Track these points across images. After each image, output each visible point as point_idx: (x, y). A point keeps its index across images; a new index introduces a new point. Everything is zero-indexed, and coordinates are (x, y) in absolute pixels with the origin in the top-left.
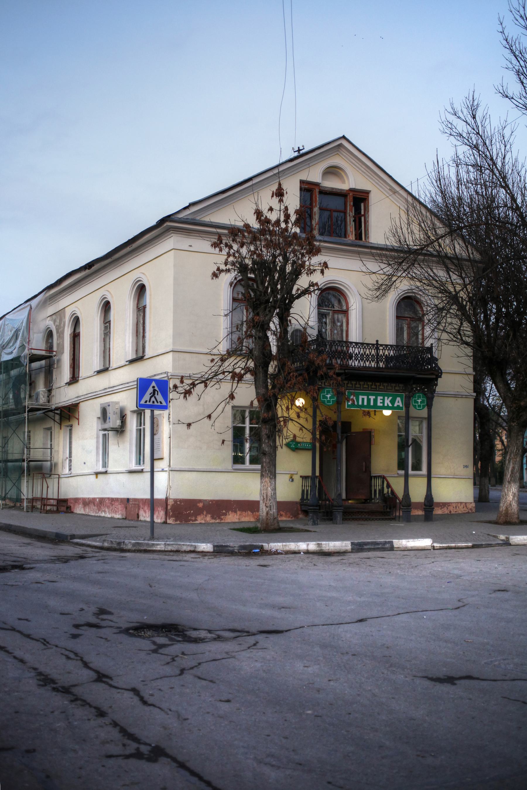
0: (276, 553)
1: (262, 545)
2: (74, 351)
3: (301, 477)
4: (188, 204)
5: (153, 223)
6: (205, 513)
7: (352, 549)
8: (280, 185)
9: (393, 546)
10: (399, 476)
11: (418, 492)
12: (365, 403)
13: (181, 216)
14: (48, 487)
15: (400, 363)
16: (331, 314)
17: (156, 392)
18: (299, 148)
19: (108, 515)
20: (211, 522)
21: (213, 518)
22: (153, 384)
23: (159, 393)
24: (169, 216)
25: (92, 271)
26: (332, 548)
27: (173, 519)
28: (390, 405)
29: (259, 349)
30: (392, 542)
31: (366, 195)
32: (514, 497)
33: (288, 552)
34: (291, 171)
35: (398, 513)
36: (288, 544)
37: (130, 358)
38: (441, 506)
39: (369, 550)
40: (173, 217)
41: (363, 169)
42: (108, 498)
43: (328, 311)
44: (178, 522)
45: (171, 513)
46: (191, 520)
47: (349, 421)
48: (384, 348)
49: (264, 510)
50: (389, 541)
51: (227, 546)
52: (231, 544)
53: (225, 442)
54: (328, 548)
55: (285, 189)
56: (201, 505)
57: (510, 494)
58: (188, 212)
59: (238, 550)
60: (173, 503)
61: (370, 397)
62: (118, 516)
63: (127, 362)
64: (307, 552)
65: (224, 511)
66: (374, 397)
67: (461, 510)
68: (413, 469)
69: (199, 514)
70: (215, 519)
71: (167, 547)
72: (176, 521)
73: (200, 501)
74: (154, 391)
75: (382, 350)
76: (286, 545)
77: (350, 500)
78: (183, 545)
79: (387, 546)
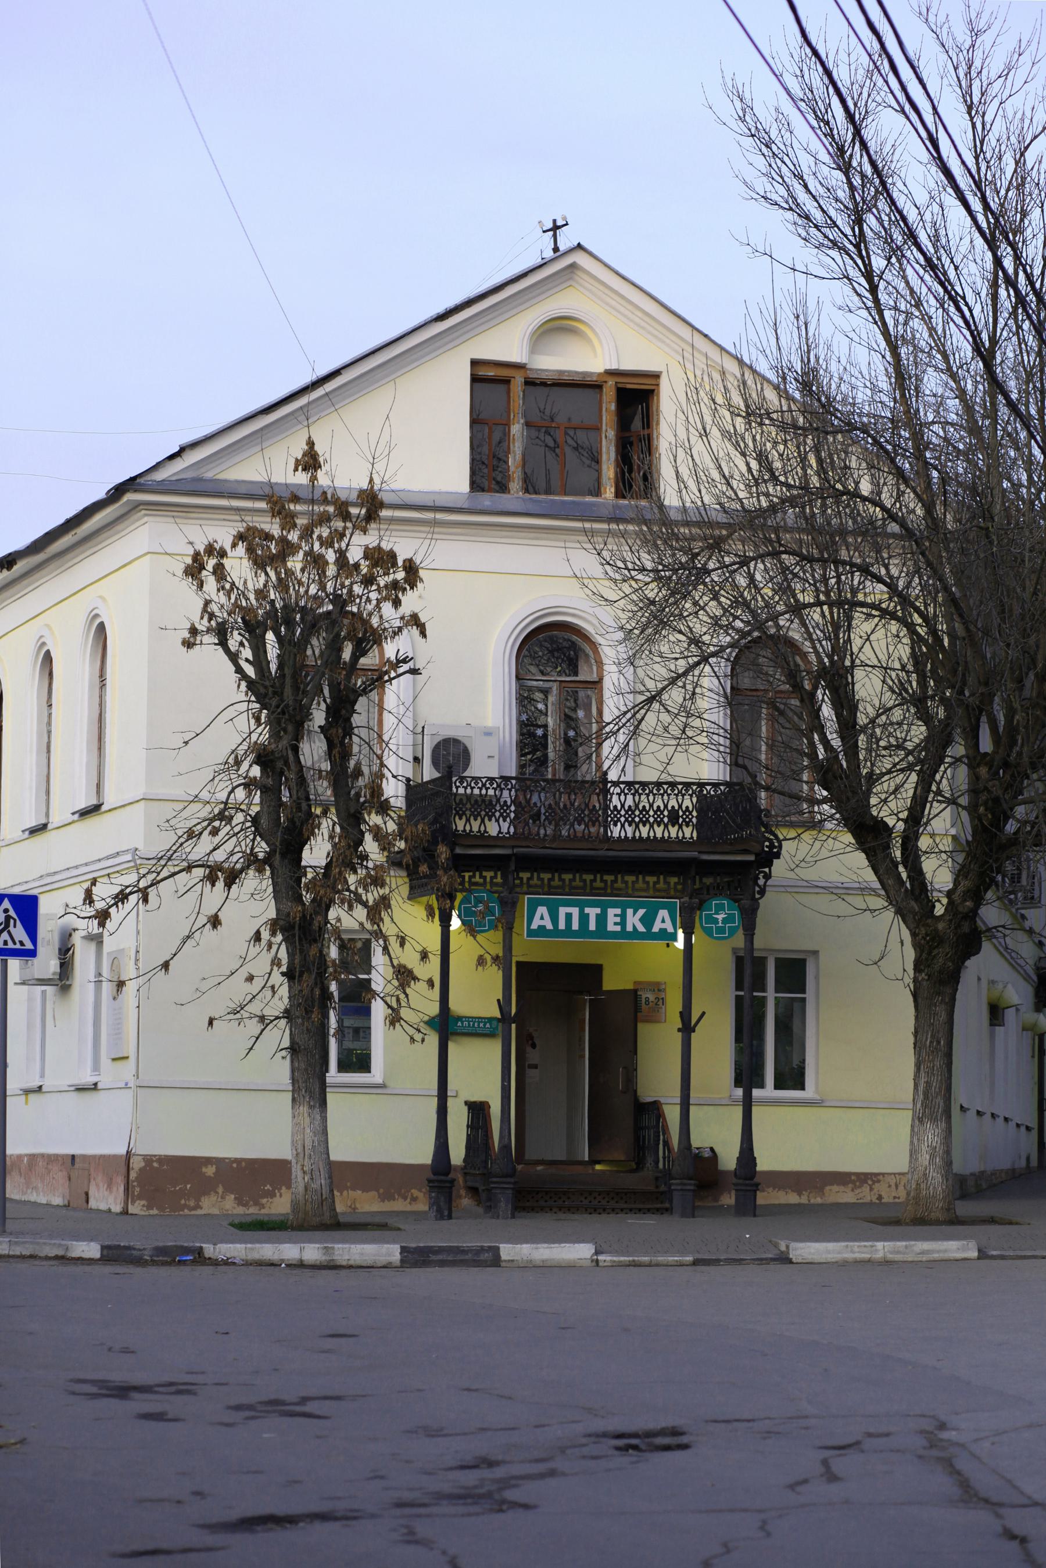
0: (227, 1263)
1: (201, 1248)
2: (100, 728)
3: (466, 1103)
4: (177, 449)
5: (100, 494)
6: (220, 1190)
7: (402, 1261)
8: (311, 444)
9: (499, 1256)
10: (733, 1102)
12: (575, 926)
13: (160, 475)
16: (554, 689)
17: (12, 921)
18: (555, 221)
19: (43, 1200)
20: (235, 1212)
21: (240, 1201)
22: (6, 904)
23: (18, 923)
24: (133, 479)
25: (17, 575)
26: (357, 1257)
27: (143, 1202)
28: (641, 928)
29: (269, 813)
30: (498, 1248)
31: (653, 382)
32: (932, 1156)
33: (260, 1263)
34: (446, 340)
35: (729, 1199)
36: (258, 1245)
37: (82, 805)
38: (853, 1182)
39: (442, 1264)
40: (141, 480)
41: (637, 320)
42: (43, 1155)
43: (547, 685)
44: (155, 1212)
45: (138, 1189)
46: (185, 1206)
47: (599, 962)
48: (622, 791)
49: (300, 1179)
50: (490, 1247)
51: (129, 1248)
52: (138, 1245)
53: (215, 1022)
54: (347, 1257)
55: (320, 453)
56: (210, 1171)
58: (179, 465)
59: (151, 1256)
60: (143, 1164)
61: (587, 910)
62: (57, 1201)
63: (73, 814)
64: (301, 1265)
65: (268, 1187)
66: (598, 910)
69: (206, 1193)
70: (245, 1205)
71: (13, 1248)
72: (149, 1207)
73: (208, 1161)
74: (8, 918)
75: (619, 795)
76: (252, 1249)
77: (599, 1162)
78: (45, 1244)
79: (486, 1256)
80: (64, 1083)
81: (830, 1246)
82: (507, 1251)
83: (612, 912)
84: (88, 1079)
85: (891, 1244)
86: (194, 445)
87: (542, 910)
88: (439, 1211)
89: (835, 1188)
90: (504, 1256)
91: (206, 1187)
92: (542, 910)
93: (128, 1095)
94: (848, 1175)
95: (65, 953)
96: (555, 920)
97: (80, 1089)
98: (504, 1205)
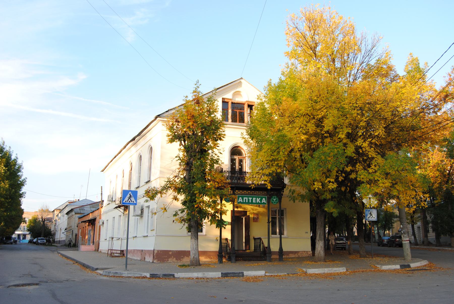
11: (275, 247)
12: (247, 201)
21: (176, 259)
22: (130, 193)
28: (260, 202)
32: (321, 248)
51: (156, 275)
56: (171, 253)
57: (319, 246)
62: (139, 259)
67: (305, 255)
68: (272, 234)
69: (170, 258)
73: (170, 251)
74: (130, 196)
79: (241, 274)
80: (141, 236)
82: (246, 273)
83: (254, 199)
84: (146, 235)
86: (171, 110)
87: (240, 198)
88: (220, 262)
90: (245, 274)
91: (169, 256)
92: (240, 198)
93: (154, 237)
94: (293, 252)
95: (142, 210)
96: (243, 200)
97: (144, 237)
98: (233, 259)
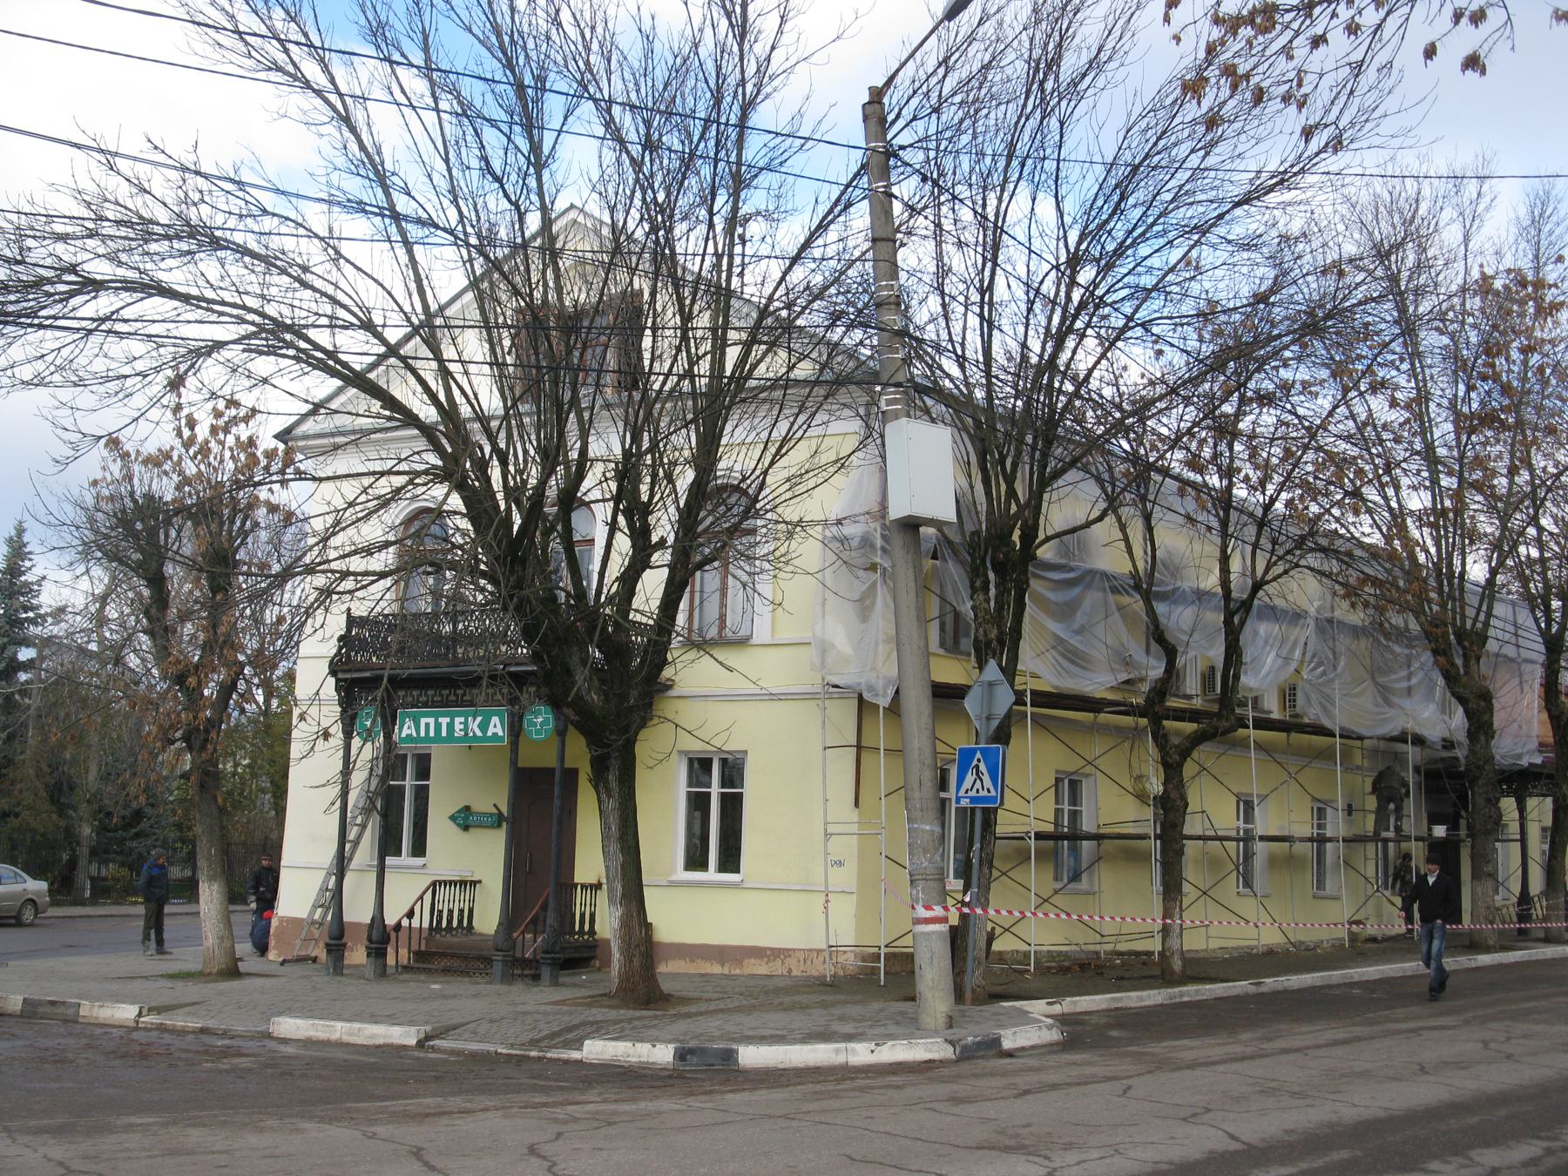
12: (432, 734)
14: (897, 1087)
15: (385, 638)
81: (300, 1022)
83: (458, 720)
85: (348, 1025)
87: (408, 722)
89: (752, 961)
92: (408, 722)
94: (765, 949)
